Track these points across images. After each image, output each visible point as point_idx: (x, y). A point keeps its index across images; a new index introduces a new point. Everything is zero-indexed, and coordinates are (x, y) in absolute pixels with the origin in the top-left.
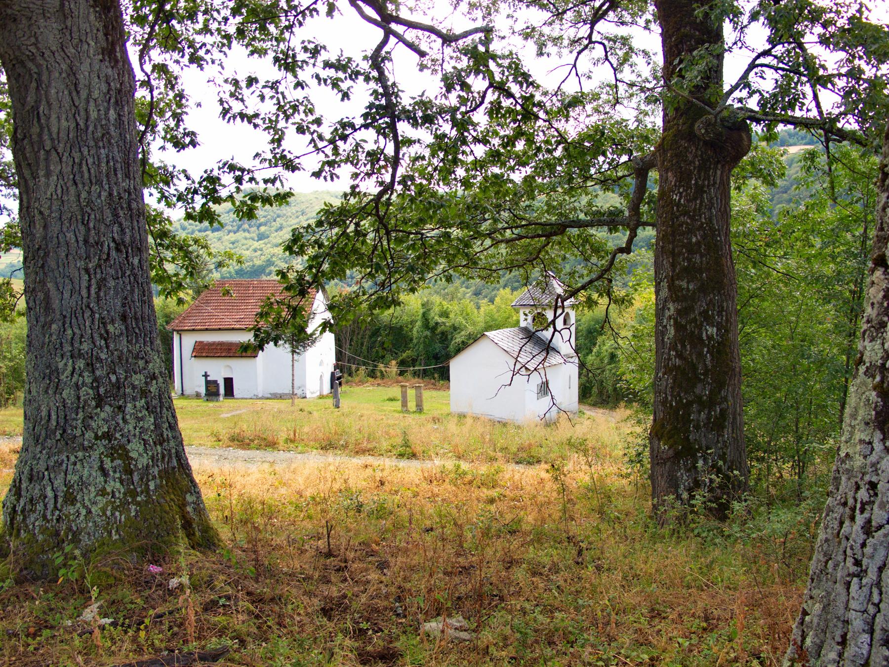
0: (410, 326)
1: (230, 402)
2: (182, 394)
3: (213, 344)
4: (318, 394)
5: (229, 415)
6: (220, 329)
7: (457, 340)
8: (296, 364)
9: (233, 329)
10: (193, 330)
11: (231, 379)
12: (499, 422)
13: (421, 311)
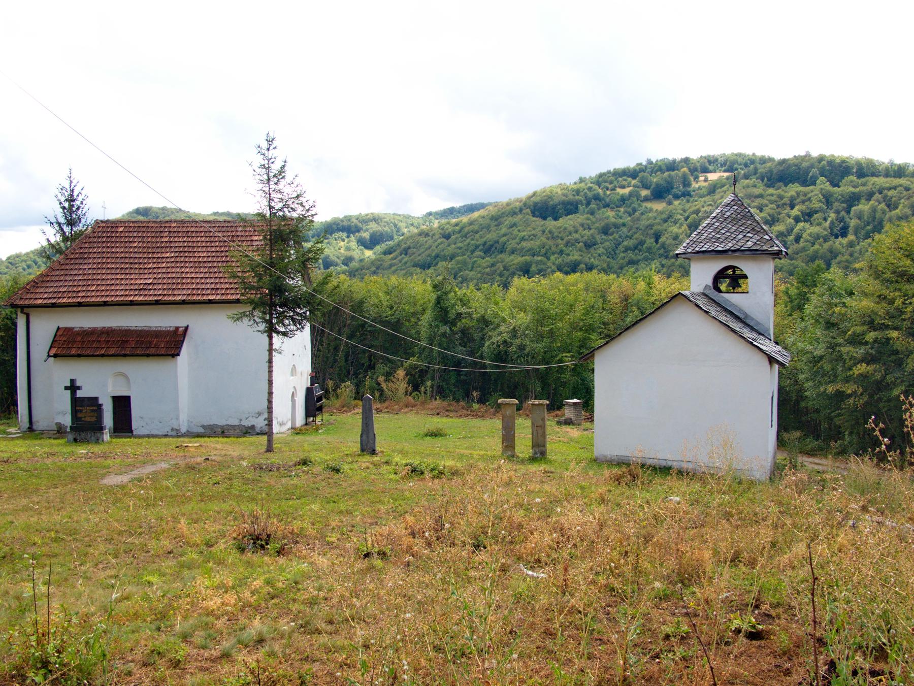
1: (124, 444)
2: (31, 429)
3: (93, 332)
4: (289, 425)
5: (124, 479)
6: (105, 304)
7: (494, 340)
8: (276, 358)
10: (54, 305)
11: (128, 399)
12: (643, 466)
13: (433, 297)
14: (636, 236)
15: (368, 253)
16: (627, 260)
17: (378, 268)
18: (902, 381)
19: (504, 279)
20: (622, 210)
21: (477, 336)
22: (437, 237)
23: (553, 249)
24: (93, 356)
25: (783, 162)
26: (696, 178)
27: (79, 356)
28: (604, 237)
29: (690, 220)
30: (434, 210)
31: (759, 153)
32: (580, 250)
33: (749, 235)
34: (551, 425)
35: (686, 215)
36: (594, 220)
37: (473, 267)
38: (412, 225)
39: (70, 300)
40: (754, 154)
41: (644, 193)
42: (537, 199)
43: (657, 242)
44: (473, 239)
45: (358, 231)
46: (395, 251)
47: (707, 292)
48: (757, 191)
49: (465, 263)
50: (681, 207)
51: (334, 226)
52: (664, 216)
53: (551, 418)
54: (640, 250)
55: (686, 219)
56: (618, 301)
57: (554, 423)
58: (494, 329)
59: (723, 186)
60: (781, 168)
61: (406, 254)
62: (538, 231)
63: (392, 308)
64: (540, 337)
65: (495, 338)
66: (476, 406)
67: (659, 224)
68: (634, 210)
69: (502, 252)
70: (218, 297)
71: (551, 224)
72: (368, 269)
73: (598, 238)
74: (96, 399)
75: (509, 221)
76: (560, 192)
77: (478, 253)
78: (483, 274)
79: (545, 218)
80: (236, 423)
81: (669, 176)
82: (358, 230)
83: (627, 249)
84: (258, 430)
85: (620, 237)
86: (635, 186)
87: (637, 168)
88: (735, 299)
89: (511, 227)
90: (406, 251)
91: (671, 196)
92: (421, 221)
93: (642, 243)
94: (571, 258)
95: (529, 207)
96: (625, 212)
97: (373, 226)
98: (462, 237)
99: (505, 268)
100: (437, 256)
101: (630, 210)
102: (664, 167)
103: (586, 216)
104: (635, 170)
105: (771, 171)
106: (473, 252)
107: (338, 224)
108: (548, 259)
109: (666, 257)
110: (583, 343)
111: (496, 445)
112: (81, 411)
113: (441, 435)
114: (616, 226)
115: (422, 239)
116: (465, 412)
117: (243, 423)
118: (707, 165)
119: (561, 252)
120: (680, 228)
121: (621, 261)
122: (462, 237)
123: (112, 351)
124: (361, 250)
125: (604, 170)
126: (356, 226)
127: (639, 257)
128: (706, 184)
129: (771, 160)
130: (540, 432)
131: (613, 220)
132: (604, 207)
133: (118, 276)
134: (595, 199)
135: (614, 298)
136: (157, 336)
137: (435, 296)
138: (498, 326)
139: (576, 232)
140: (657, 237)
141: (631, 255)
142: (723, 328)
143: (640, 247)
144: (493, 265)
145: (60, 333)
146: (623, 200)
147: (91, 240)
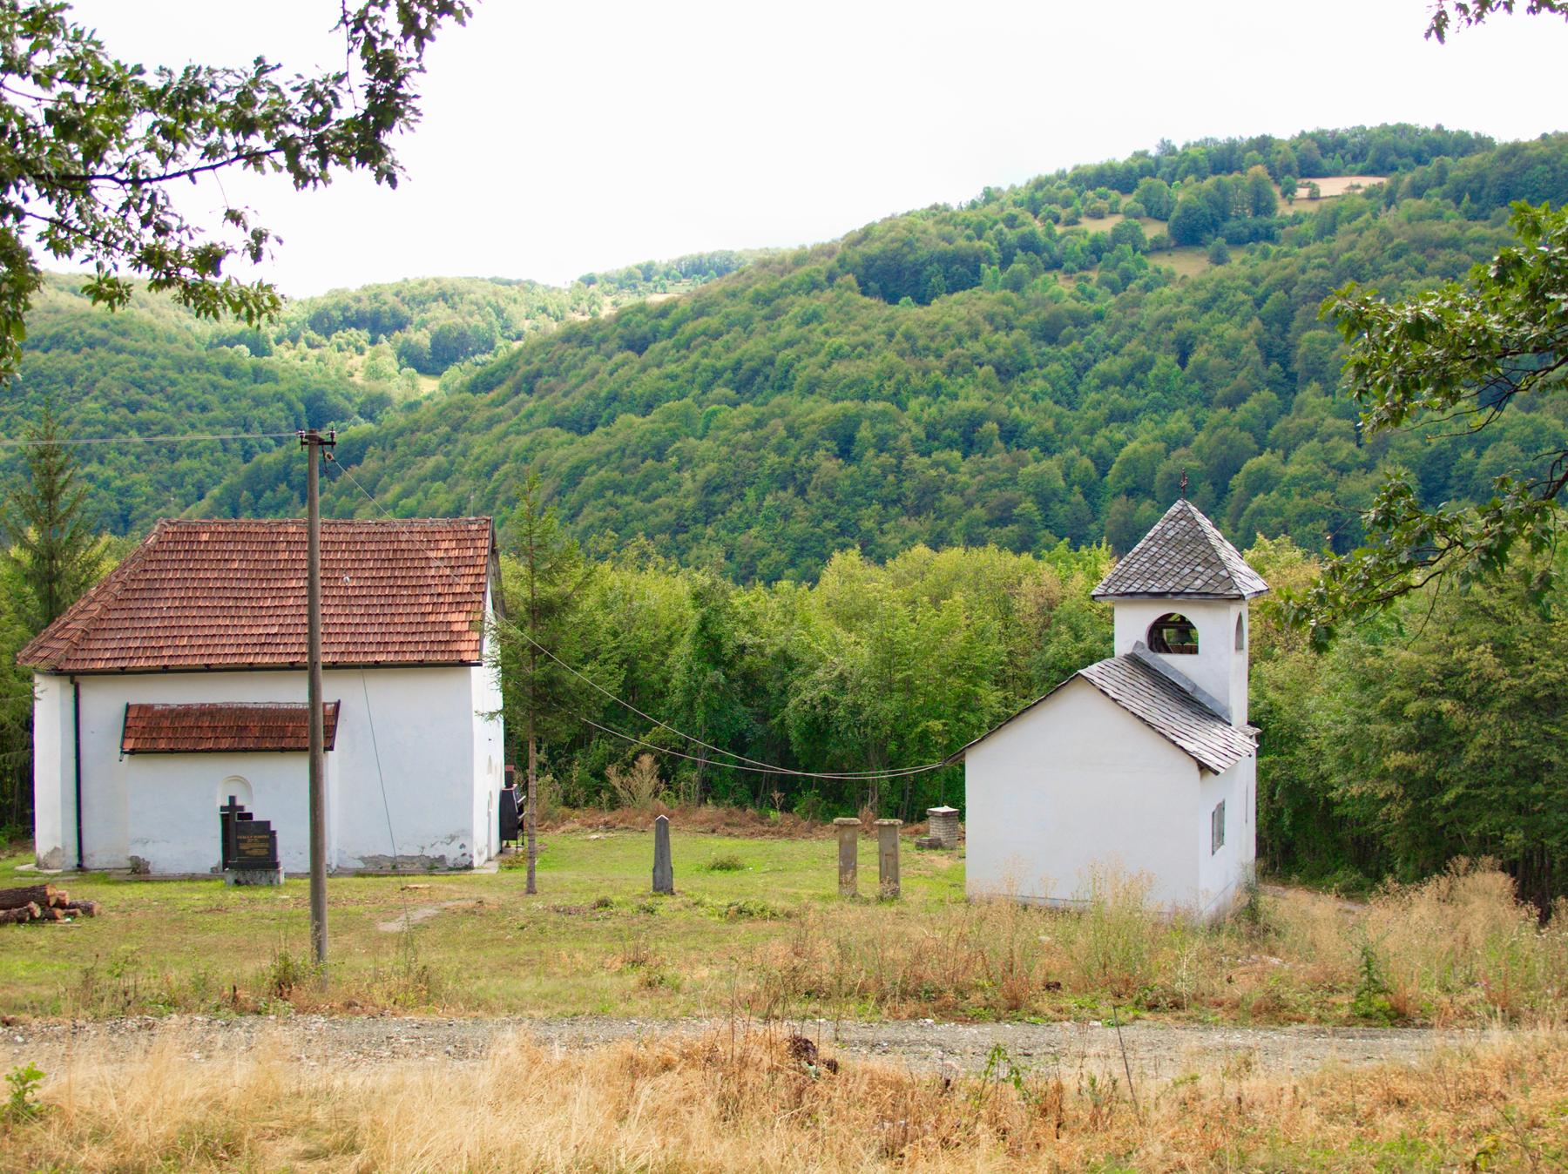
0: (655, 657)
3: (186, 712)
6: (208, 669)
7: (806, 695)
9: (251, 668)
10: (123, 671)
13: (693, 617)
14: (1129, 347)
15: (428, 385)
16: (1105, 409)
17: (455, 429)
18: (1461, 780)
19: (789, 459)
20: (1094, 275)
21: (773, 686)
22: (613, 345)
23: (916, 380)
24: (195, 751)
25: (1515, 150)
26: (1288, 192)
27: (172, 751)
28: (1047, 349)
29: (1268, 306)
30: (598, 270)
31: (1452, 126)
32: (985, 384)
33: (1200, 569)
34: (906, 847)
35: (1260, 291)
36: (1021, 304)
37: (707, 427)
38: (544, 310)
39: (151, 663)
40: (1439, 128)
41: (1153, 230)
42: (874, 248)
43: (1183, 362)
44: (705, 355)
45: (401, 326)
46: (501, 382)
47: (1139, 652)
48: (1443, 230)
49: (687, 418)
50: (1245, 270)
51: (336, 314)
52: (1202, 295)
53: (907, 837)
54: (1140, 385)
55: (1259, 303)
56: (1034, 610)
57: (911, 846)
58: (805, 675)
59: (1359, 214)
60: (1508, 169)
61: (530, 391)
62: (876, 336)
63: (615, 635)
64: (887, 689)
65: (808, 692)
66: (775, 815)
67: (1190, 315)
68: (1127, 278)
69: (782, 388)
70: (391, 657)
71: (908, 313)
72: (430, 429)
73: (1031, 351)
74: (268, 823)
75: (801, 304)
76: (933, 230)
77: (719, 391)
78: (735, 447)
79: (893, 299)
80: (416, 853)
81: (1218, 186)
82: (401, 324)
83: (1106, 382)
84: (450, 863)
85: (1090, 349)
86: (1128, 213)
87: (1135, 165)
88: (1176, 663)
89: (806, 322)
90: (529, 384)
91: (1220, 241)
92: (567, 300)
93: (1145, 365)
94: (961, 404)
95: (853, 271)
96: (1104, 282)
97: (441, 316)
98: (677, 347)
99: (792, 432)
100: (613, 397)
101: (1114, 276)
102: (1204, 163)
103: (999, 294)
104: (1130, 171)
105: (1481, 177)
106: (707, 387)
107: (346, 308)
108: (902, 407)
109: (1208, 403)
110: (966, 702)
111: (830, 881)
112: (245, 841)
113: (737, 868)
114: (1079, 321)
115: (571, 352)
116: (759, 827)
117: (426, 853)
118: (1320, 154)
119: (937, 390)
120: (1242, 326)
121: (1091, 413)
122: (677, 347)
123: (225, 744)
124: (410, 377)
125: (1050, 171)
126: (394, 314)
127: (1137, 403)
128: (1312, 208)
129: (1483, 144)
130: (891, 862)
131: (1072, 304)
132: (1048, 268)
133: (220, 622)
134: (1025, 249)
135: (1026, 604)
136: (292, 719)
137: (698, 617)
138: (813, 668)
139: (975, 336)
140: (1183, 351)
141: (1114, 396)
142: (1138, 722)
143: (1138, 376)
144: (760, 423)
145: (133, 714)
146: (1097, 250)
147: (160, 556)
